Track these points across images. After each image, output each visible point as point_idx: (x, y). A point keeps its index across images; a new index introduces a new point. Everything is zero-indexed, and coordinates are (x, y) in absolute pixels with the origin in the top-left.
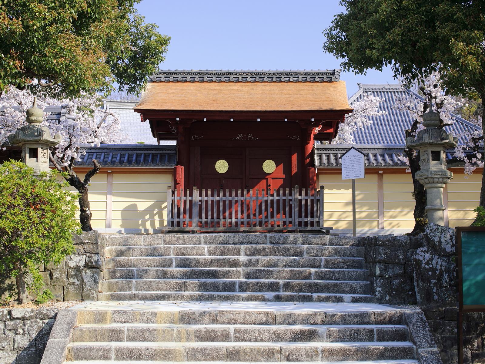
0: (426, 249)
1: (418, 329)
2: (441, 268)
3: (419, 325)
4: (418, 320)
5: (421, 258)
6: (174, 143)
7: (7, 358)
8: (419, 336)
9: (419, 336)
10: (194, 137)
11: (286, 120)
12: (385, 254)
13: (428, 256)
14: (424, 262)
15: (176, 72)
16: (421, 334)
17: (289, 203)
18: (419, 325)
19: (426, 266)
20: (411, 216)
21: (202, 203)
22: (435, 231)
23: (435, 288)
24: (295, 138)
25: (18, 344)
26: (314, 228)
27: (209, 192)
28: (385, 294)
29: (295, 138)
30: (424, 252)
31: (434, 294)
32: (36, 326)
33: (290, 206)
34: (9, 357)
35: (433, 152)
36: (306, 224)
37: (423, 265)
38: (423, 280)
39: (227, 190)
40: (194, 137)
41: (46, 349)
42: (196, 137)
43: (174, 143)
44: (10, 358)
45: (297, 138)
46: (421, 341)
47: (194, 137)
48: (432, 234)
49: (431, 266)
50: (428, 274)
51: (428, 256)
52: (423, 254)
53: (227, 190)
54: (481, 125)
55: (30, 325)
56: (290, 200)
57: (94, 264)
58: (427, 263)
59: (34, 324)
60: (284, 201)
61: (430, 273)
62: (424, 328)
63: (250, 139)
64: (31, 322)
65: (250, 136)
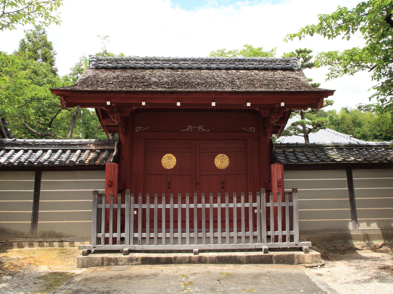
10: (138, 129)
15: (137, 58)
17: (253, 211)
21: (137, 212)
24: (250, 129)
27: (140, 198)
28: (389, 74)
29: (250, 129)
37: (325, 99)
39: (156, 195)
40: (138, 129)
42: (141, 129)
45: (253, 129)
47: (138, 129)
53: (156, 195)
54: (315, 279)
56: (254, 208)
60: (247, 209)
63: (200, 132)
65: (200, 127)
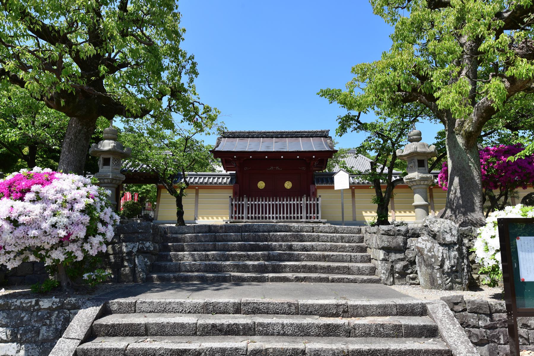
0: (426, 238)
1: (448, 326)
2: (443, 256)
3: (447, 321)
4: (444, 314)
5: (424, 246)
6: (235, 172)
7: (30, 351)
8: (451, 337)
9: (451, 337)
11: (298, 157)
12: (388, 242)
13: (429, 245)
14: (426, 250)
16: (453, 334)
18: (447, 321)
19: (429, 254)
20: (375, 214)
22: (434, 222)
23: (438, 274)
25: (43, 335)
26: (316, 220)
30: (425, 240)
31: (438, 279)
32: (62, 317)
33: (301, 207)
34: (32, 349)
35: (419, 161)
36: (311, 218)
37: (426, 252)
38: (427, 266)
41: (53, 350)
43: (235, 172)
44: (33, 351)
46: (456, 343)
48: (431, 225)
49: (433, 253)
50: (431, 261)
51: (429, 245)
52: (424, 242)
55: (57, 315)
57: (145, 249)
58: (429, 251)
59: (61, 314)
61: (433, 260)
62: (454, 324)
64: (58, 313)
